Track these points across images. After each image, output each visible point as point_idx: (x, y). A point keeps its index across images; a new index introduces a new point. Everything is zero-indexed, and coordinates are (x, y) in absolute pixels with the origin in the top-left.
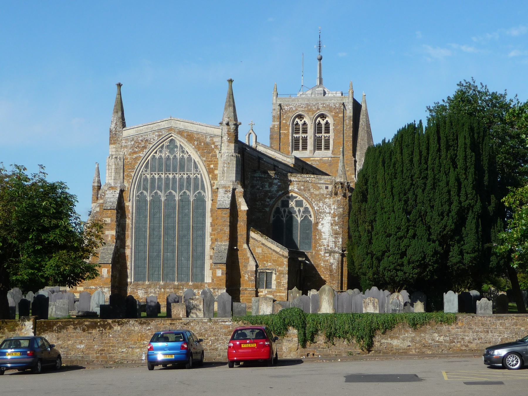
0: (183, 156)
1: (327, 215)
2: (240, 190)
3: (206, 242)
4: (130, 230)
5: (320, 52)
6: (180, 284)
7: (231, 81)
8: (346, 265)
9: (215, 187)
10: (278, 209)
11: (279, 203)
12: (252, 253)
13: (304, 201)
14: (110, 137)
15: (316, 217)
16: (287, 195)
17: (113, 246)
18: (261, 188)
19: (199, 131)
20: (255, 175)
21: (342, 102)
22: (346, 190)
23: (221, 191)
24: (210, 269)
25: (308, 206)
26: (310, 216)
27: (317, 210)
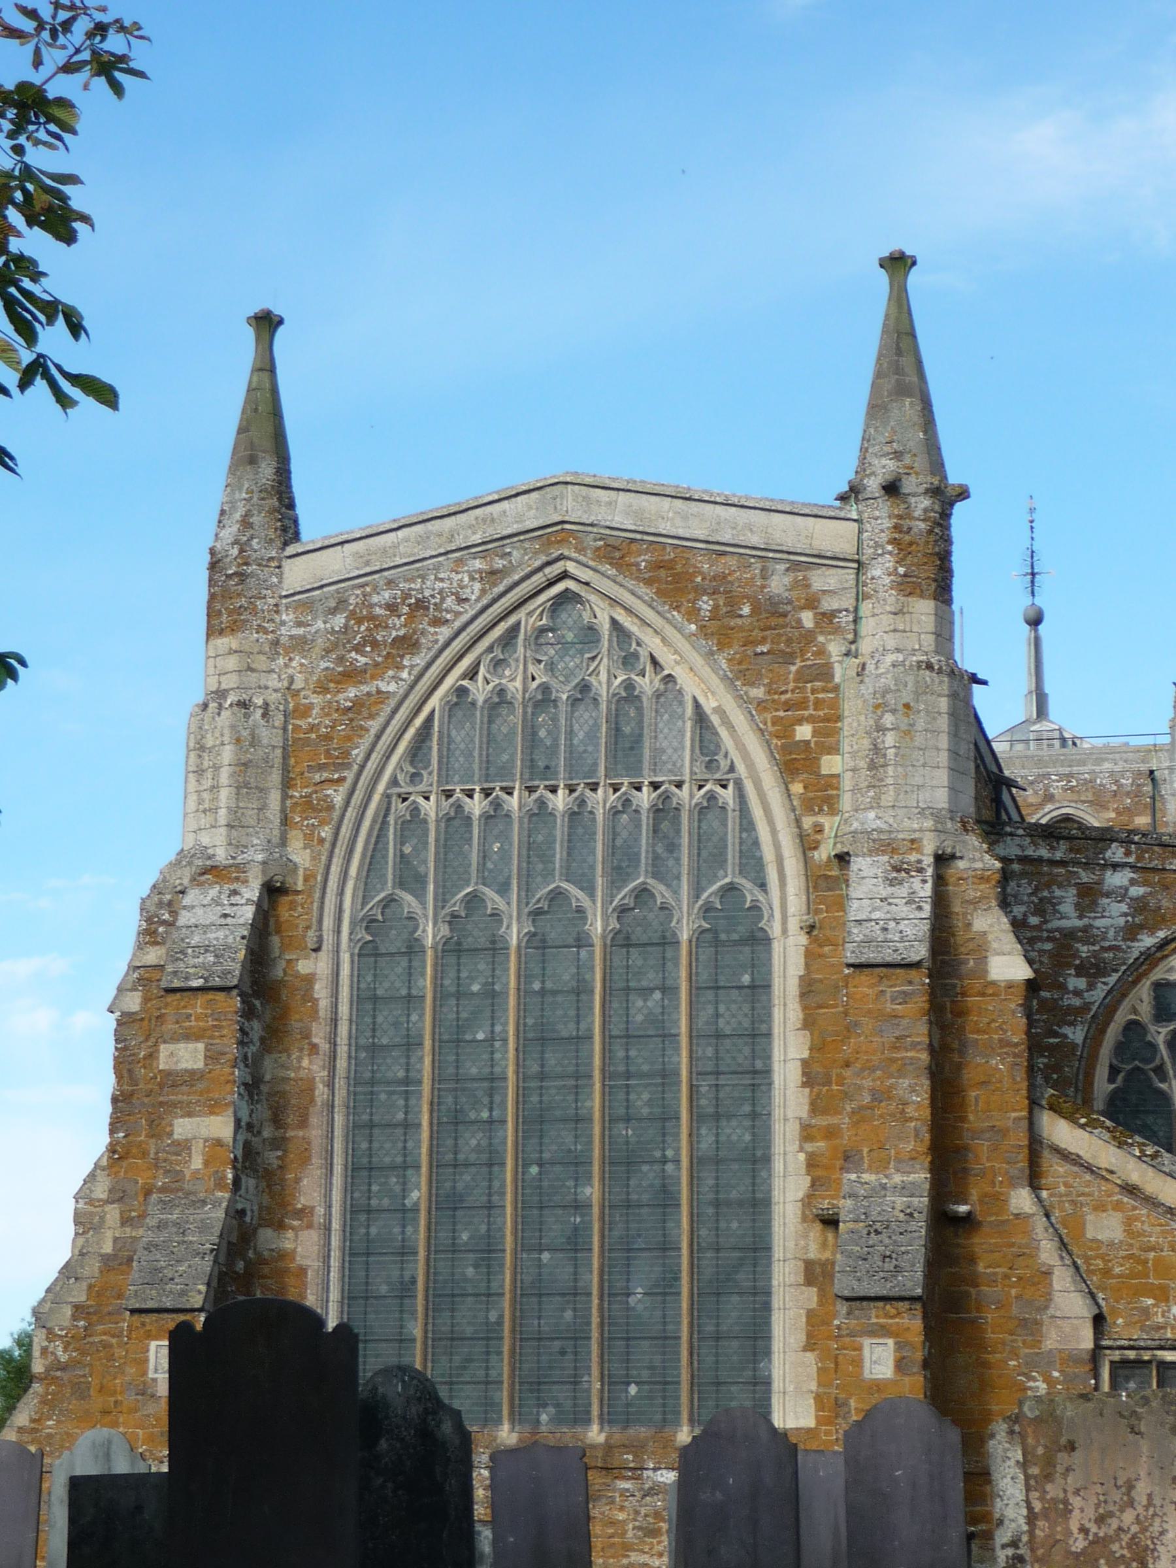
0: (629, 686)
3: (777, 1183)
4: (316, 1120)
5: (1033, 593)
6: (618, 1437)
7: (898, 264)
10: (1133, 1028)
14: (212, 597)
17: (216, 1204)
18: (1034, 920)
19: (727, 537)
21: (1144, 768)
23: (867, 870)
24: (809, 1347)
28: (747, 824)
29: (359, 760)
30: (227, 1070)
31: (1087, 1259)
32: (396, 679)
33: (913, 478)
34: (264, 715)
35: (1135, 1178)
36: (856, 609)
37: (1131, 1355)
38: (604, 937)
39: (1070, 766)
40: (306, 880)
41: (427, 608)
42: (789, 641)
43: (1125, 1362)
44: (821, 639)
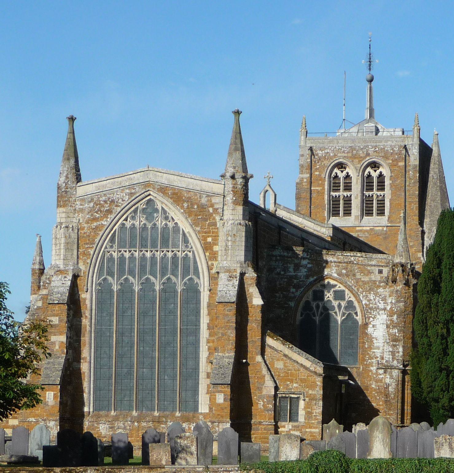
0: (166, 225)
1: (381, 312)
2: (251, 274)
5: (370, 69)
6: (162, 414)
7: (238, 113)
8: (409, 387)
9: (214, 271)
10: (308, 303)
11: (310, 295)
12: (269, 369)
13: (347, 292)
14: (58, 197)
15: (364, 315)
16: (322, 283)
17: (62, 358)
18: (282, 273)
19: (191, 187)
20: (274, 253)
21: (403, 144)
22: (409, 275)
23: (223, 277)
24: (207, 393)
25: (353, 299)
26: (356, 313)
27: (366, 304)
28: (195, 262)
29: (97, 242)
30: (64, 324)
31: (275, 372)
32: (107, 221)
33: (238, 174)
34: (72, 230)
35: (287, 353)
36: (223, 208)
37: (284, 395)
38: (159, 290)
39: (376, 143)
40: (84, 273)
41: (114, 202)
42: (206, 215)
43: (282, 397)
44: (214, 215)
